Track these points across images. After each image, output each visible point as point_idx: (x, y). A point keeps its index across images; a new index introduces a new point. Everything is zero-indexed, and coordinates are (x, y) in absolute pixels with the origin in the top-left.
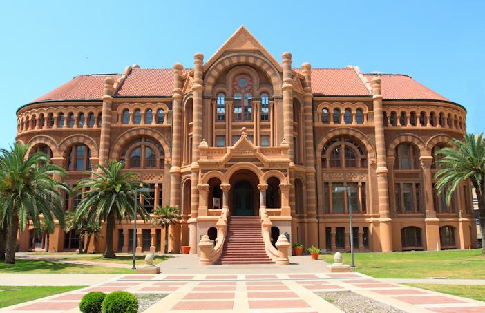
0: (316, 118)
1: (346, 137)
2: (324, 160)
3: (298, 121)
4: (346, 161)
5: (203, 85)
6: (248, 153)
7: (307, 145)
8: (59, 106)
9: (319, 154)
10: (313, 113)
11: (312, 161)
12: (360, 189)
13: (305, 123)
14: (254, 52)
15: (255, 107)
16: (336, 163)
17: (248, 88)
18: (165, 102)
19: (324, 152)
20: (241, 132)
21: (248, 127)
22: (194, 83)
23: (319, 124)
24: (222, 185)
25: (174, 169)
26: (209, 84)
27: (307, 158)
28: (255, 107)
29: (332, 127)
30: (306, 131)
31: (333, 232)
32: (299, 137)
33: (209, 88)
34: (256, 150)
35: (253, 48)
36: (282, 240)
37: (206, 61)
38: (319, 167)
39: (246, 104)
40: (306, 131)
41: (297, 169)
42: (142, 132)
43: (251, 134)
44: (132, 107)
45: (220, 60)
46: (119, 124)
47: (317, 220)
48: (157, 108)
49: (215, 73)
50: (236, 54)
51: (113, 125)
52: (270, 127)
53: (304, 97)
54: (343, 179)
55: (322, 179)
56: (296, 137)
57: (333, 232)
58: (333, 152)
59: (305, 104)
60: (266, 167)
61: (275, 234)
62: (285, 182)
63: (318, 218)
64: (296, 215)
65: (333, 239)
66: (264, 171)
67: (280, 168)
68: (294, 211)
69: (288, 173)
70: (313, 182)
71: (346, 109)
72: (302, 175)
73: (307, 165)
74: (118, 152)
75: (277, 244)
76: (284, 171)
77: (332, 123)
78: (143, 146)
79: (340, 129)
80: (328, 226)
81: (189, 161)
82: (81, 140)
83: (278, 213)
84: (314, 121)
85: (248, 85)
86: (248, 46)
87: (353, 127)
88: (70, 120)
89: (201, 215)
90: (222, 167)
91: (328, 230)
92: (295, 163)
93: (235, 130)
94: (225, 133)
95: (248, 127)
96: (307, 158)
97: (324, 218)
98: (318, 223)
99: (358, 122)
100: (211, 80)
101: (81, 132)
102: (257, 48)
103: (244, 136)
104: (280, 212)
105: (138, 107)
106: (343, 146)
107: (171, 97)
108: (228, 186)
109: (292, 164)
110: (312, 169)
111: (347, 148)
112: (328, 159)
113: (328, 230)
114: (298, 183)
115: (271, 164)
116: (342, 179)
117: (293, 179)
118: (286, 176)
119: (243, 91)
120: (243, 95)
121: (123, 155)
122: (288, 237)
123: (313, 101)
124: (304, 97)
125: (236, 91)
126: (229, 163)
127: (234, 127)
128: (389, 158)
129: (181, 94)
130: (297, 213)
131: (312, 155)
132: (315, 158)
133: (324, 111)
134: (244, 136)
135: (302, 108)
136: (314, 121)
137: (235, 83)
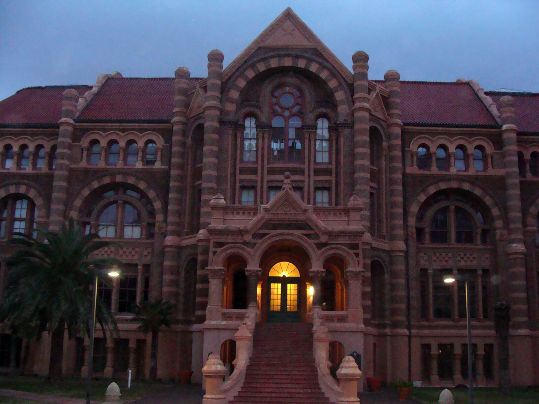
0: (408, 161)
1: (459, 192)
2: (420, 232)
3: (379, 183)
4: (458, 234)
5: (221, 101)
6: (290, 215)
7: (393, 205)
8: (146, 130)
9: (412, 221)
10: (403, 152)
11: (400, 232)
12: (480, 280)
13: (180, 216)
14: (306, 50)
15: (307, 141)
16: (439, 236)
17: (295, 110)
18: (158, 131)
19: (420, 217)
20: (282, 181)
21: (294, 171)
22: (209, 101)
23: (413, 169)
24: (248, 268)
25: (169, 240)
26: (231, 100)
27: (393, 228)
28: (307, 141)
29: (434, 176)
30: (392, 182)
31: (435, 351)
32: (378, 190)
33: (231, 107)
34: (305, 211)
35: (306, 43)
36: (349, 367)
37: (226, 63)
38: (412, 243)
39: (292, 134)
40: (392, 182)
41: (375, 244)
42: (119, 178)
43: (298, 185)
44: (123, 137)
45: (249, 63)
46: (83, 164)
47: (406, 331)
48: (144, 140)
49: (242, 83)
50: (276, 53)
51: (73, 166)
52: (331, 175)
53: (389, 126)
54: (475, 263)
55: (418, 263)
56: (374, 191)
57: (435, 351)
58: (435, 220)
59: (389, 137)
60: (324, 239)
61: (335, 360)
62: (354, 266)
63: (409, 327)
64: (373, 322)
65: (434, 364)
66: (320, 246)
67: (343, 242)
68: (368, 316)
69: (360, 251)
70: (401, 267)
71: (457, 147)
72: (383, 255)
73: (393, 238)
74: (80, 211)
75: (342, 371)
76: (354, 246)
77: (434, 170)
78: (120, 202)
79: (449, 179)
80: (426, 341)
81: (195, 228)
82: (22, 190)
83: (342, 319)
84: (404, 165)
85: (297, 104)
86: (297, 41)
87: (469, 176)
88: (20, 156)
89: (212, 319)
90: (248, 238)
91: (426, 347)
92: (373, 235)
93: (272, 177)
94: (256, 181)
95: (294, 171)
96: (393, 228)
97: (420, 327)
98: (410, 337)
99: (439, 168)
100: (235, 94)
101: (23, 176)
102: (311, 44)
103: (287, 186)
104: (346, 316)
105: (114, 137)
106: (452, 207)
107: (168, 121)
108: (257, 271)
109: (367, 237)
110: (401, 245)
111: (458, 209)
112: (427, 230)
113: (426, 347)
114: (376, 268)
115: (330, 234)
116: (451, 263)
117: (369, 262)
118: (357, 255)
119: (287, 113)
120: (286, 119)
121: (89, 215)
122: (358, 359)
123: (403, 131)
124: (389, 126)
125: (275, 114)
126: (261, 231)
127: (271, 171)
128: (529, 228)
129: (186, 117)
130: (373, 318)
131: (401, 222)
132: (406, 226)
133: (420, 149)
134: (287, 186)
135: (385, 144)
136: (404, 165)
137: (274, 100)
